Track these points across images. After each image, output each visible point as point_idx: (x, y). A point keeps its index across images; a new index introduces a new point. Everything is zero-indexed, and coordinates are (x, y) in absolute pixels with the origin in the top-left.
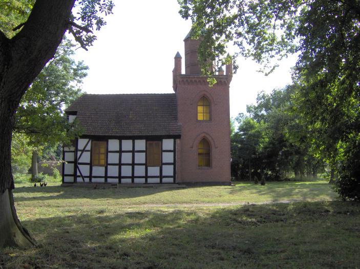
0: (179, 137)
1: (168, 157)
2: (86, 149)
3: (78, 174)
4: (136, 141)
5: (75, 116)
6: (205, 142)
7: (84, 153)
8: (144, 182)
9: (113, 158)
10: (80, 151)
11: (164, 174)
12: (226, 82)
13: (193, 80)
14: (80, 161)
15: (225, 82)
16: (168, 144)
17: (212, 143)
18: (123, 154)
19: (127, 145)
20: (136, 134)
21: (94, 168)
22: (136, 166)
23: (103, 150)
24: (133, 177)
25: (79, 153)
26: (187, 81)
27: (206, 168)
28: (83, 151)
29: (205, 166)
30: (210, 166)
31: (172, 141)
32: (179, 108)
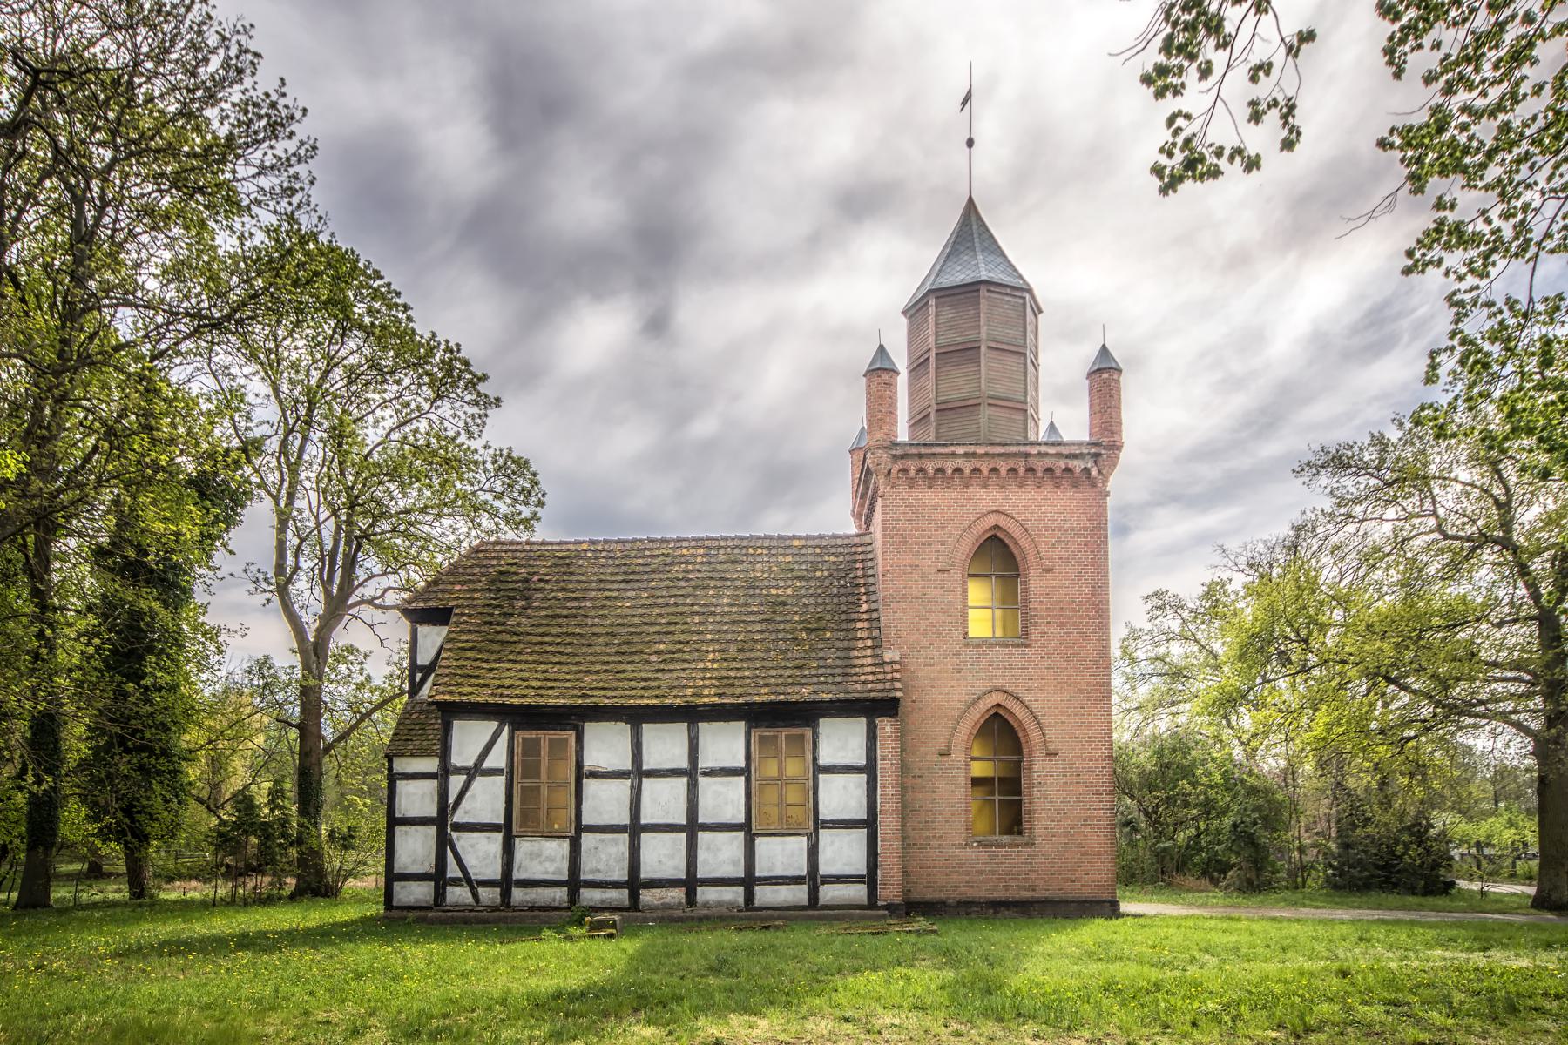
0: (887, 707)
1: (842, 796)
2: (487, 764)
3: (453, 871)
4: (703, 726)
5: (443, 631)
6: (1001, 731)
7: (479, 782)
8: (805, 902)
9: (605, 801)
10: (459, 771)
11: (646, 873)
12: (1094, 472)
13: (949, 466)
14: (459, 817)
15: (1086, 470)
16: (841, 741)
17: (1034, 735)
18: (647, 783)
19: (665, 745)
20: (709, 697)
21: (523, 847)
22: (703, 837)
23: (567, 772)
24: (691, 883)
25: (456, 782)
26: (921, 470)
27: (1007, 839)
28: (476, 770)
29: (1003, 833)
30: (1020, 833)
31: (858, 725)
32: (883, 589)
